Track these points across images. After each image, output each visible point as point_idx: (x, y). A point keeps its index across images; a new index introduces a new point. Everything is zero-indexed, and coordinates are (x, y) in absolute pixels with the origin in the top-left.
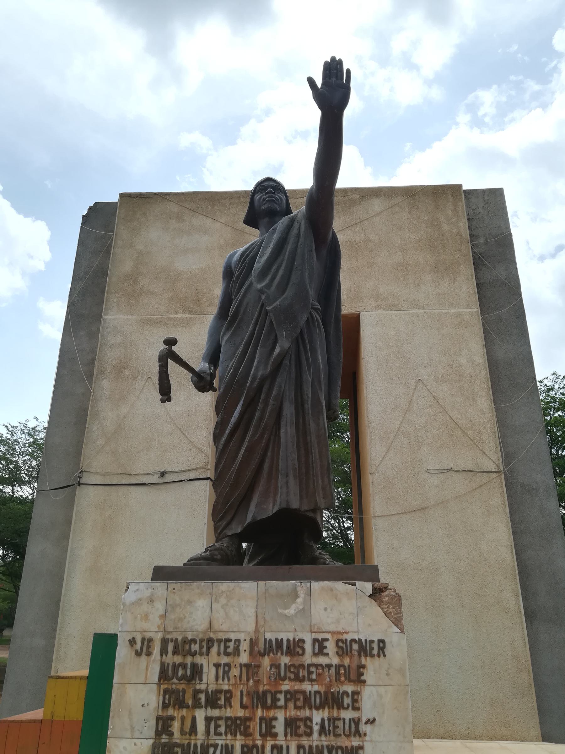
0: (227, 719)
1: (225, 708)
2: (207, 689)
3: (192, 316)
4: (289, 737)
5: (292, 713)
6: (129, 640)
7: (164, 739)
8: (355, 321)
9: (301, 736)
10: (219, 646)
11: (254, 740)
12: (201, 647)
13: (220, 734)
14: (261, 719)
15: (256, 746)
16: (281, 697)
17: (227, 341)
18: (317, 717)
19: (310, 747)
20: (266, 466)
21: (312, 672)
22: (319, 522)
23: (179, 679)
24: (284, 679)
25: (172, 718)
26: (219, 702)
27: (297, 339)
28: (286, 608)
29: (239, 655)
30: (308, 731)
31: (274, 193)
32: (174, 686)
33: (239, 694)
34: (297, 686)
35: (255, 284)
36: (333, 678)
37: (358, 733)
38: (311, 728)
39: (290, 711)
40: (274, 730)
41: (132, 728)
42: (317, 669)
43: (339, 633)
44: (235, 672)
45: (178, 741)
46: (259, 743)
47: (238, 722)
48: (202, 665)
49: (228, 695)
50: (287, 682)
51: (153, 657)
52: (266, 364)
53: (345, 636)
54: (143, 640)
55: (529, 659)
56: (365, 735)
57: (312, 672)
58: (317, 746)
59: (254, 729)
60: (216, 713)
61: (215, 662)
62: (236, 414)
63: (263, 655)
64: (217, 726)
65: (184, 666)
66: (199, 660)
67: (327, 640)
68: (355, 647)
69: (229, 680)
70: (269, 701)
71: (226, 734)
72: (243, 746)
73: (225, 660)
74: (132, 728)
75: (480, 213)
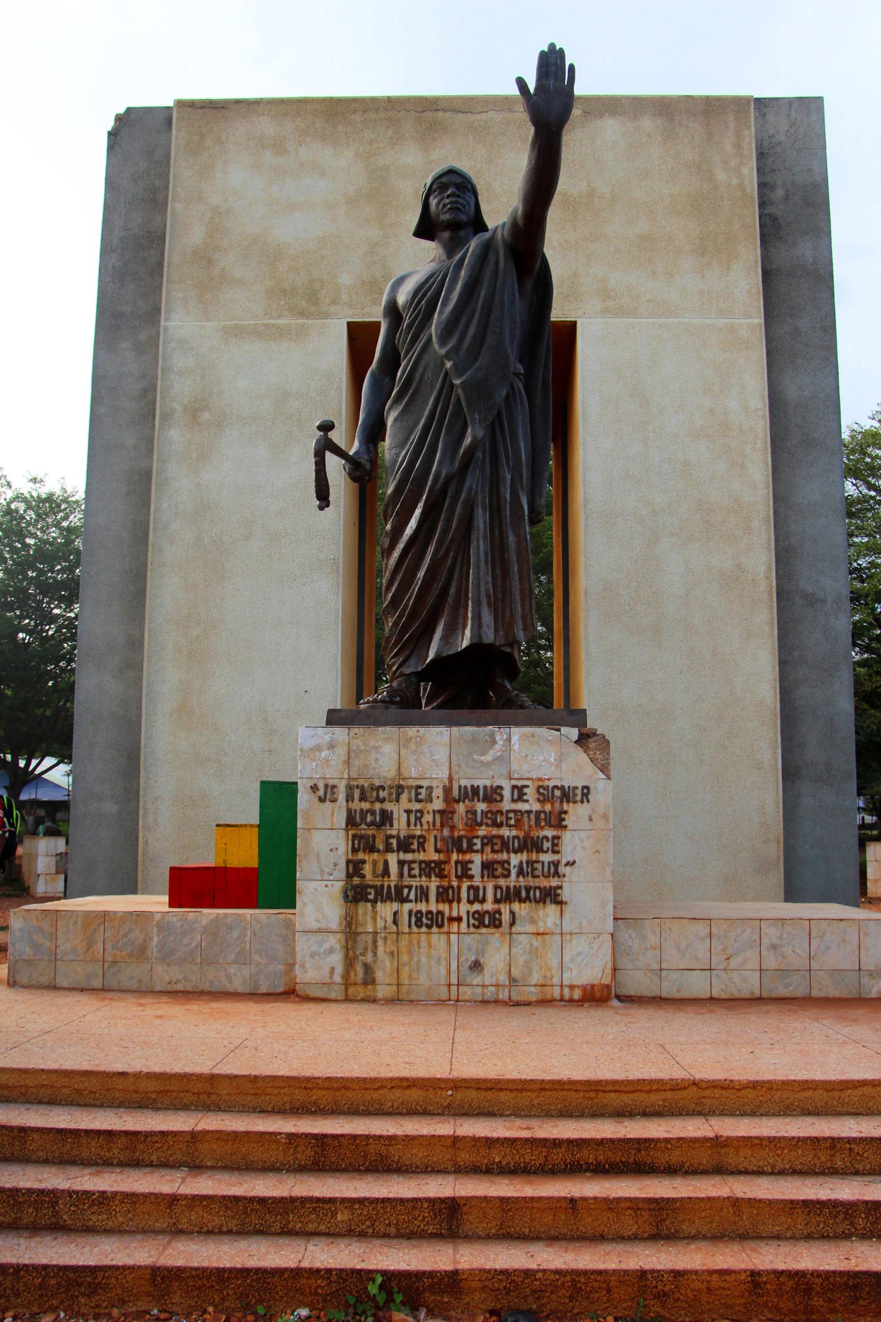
0: (421, 862)
1: (419, 851)
2: (398, 834)
3: (306, 321)
4: (485, 879)
5: (490, 856)
6: (311, 787)
7: (356, 880)
8: (569, 330)
9: (498, 877)
10: (410, 793)
11: (450, 881)
12: (390, 795)
13: (415, 876)
14: (457, 862)
15: (452, 887)
16: (478, 842)
17: (395, 420)
18: (515, 860)
19: (508, 888)
20: (452, 591)
21: (511, 818)
22: (517, 658)
23: (368, 825)
24: (481, 825)
25: (364, 862)
26: (412, 847)
27: (493, 423)
28: (483, 754)
29: (431, 801)
30: (506, 873)
31: (458, 196)
32: (363, 832)
33: (432, 839)
34: (495, 831)
35: (435, 345)
36: (533, 823)
37: (557, 874)
38: (509, 871)
39: (487, 855)
40: (470, 873)
41: (322, 871)
42: (516, 815)
43: (540, 779)
44: (428, 818)
45: (371, 883)
46: (455, 884)
47: (433, 865)
48: (392, 811)
49: (421, 840)
50: (483, 827)
51: (338, 803)
52: (453, 459)
53: (547, 783)
54: (326, 786)
55: (781, 826)
56: (564, 876)
57: (511, 818)
58: (515, 887)
59: (449, 871)
60: (409, 857)
61: (406, 808)
62: (413, 524)
63: (458, 802)
64: (410, 869)
65: (373, 813)
66: (389, 806)
67: (527, 786)
68: (558, 793)
69: (421, 825)
70: (465, 845)
71: (420, 876)
72: (438, 887)
73: (417, 806)
74: (322, 871)
75: (780, 143)
